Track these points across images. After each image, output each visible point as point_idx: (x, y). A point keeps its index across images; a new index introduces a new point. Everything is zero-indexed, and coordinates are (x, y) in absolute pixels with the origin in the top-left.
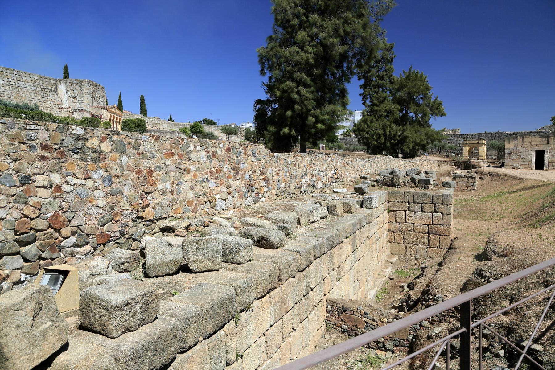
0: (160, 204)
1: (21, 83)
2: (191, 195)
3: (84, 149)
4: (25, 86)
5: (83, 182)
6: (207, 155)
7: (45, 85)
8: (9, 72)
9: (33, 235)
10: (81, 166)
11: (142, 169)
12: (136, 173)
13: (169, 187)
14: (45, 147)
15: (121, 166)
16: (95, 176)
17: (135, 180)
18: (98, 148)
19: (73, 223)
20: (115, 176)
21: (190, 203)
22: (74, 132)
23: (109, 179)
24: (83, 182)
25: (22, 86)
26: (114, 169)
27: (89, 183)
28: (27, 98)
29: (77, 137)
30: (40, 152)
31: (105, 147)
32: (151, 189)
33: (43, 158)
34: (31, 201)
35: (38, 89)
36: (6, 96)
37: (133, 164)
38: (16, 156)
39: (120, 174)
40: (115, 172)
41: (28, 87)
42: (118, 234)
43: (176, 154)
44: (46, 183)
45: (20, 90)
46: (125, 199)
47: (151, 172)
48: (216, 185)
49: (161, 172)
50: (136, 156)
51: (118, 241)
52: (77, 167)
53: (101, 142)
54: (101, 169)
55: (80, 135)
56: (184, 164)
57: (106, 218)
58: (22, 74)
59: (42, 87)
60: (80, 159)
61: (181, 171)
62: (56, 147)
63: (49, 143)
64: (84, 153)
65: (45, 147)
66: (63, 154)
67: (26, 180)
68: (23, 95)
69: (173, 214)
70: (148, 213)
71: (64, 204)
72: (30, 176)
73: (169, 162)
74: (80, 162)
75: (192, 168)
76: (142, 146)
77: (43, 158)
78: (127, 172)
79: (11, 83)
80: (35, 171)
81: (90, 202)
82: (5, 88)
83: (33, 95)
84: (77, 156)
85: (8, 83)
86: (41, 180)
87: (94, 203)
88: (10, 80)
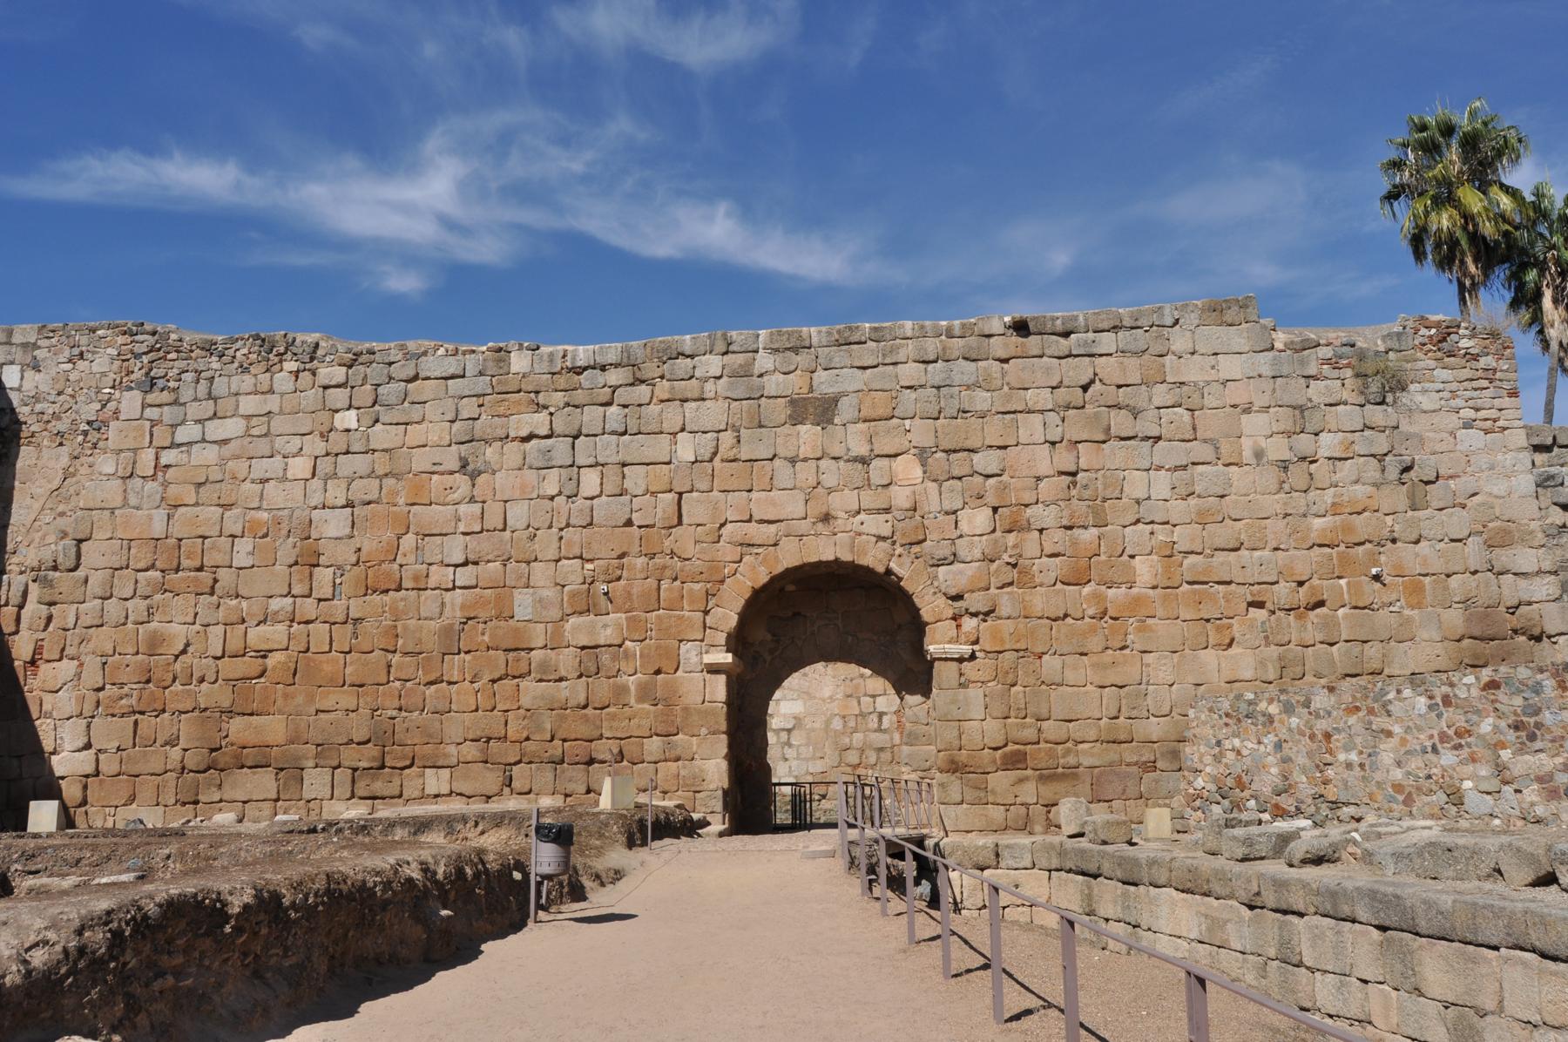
2: (1398, 774)
14: (1227, 715)
15: (1290, 730)
19: (1253, 786)
21: (1398, 788)
23: (1278, 746)
27: (1262, 748)
29: (1250, 703)
47: (1328, 736)
56: (1380, 722)
66: (1239, 720)
67: (1219, 743)
70: (1332, 793)
73: (1352, 720)
75: (1397, 729)
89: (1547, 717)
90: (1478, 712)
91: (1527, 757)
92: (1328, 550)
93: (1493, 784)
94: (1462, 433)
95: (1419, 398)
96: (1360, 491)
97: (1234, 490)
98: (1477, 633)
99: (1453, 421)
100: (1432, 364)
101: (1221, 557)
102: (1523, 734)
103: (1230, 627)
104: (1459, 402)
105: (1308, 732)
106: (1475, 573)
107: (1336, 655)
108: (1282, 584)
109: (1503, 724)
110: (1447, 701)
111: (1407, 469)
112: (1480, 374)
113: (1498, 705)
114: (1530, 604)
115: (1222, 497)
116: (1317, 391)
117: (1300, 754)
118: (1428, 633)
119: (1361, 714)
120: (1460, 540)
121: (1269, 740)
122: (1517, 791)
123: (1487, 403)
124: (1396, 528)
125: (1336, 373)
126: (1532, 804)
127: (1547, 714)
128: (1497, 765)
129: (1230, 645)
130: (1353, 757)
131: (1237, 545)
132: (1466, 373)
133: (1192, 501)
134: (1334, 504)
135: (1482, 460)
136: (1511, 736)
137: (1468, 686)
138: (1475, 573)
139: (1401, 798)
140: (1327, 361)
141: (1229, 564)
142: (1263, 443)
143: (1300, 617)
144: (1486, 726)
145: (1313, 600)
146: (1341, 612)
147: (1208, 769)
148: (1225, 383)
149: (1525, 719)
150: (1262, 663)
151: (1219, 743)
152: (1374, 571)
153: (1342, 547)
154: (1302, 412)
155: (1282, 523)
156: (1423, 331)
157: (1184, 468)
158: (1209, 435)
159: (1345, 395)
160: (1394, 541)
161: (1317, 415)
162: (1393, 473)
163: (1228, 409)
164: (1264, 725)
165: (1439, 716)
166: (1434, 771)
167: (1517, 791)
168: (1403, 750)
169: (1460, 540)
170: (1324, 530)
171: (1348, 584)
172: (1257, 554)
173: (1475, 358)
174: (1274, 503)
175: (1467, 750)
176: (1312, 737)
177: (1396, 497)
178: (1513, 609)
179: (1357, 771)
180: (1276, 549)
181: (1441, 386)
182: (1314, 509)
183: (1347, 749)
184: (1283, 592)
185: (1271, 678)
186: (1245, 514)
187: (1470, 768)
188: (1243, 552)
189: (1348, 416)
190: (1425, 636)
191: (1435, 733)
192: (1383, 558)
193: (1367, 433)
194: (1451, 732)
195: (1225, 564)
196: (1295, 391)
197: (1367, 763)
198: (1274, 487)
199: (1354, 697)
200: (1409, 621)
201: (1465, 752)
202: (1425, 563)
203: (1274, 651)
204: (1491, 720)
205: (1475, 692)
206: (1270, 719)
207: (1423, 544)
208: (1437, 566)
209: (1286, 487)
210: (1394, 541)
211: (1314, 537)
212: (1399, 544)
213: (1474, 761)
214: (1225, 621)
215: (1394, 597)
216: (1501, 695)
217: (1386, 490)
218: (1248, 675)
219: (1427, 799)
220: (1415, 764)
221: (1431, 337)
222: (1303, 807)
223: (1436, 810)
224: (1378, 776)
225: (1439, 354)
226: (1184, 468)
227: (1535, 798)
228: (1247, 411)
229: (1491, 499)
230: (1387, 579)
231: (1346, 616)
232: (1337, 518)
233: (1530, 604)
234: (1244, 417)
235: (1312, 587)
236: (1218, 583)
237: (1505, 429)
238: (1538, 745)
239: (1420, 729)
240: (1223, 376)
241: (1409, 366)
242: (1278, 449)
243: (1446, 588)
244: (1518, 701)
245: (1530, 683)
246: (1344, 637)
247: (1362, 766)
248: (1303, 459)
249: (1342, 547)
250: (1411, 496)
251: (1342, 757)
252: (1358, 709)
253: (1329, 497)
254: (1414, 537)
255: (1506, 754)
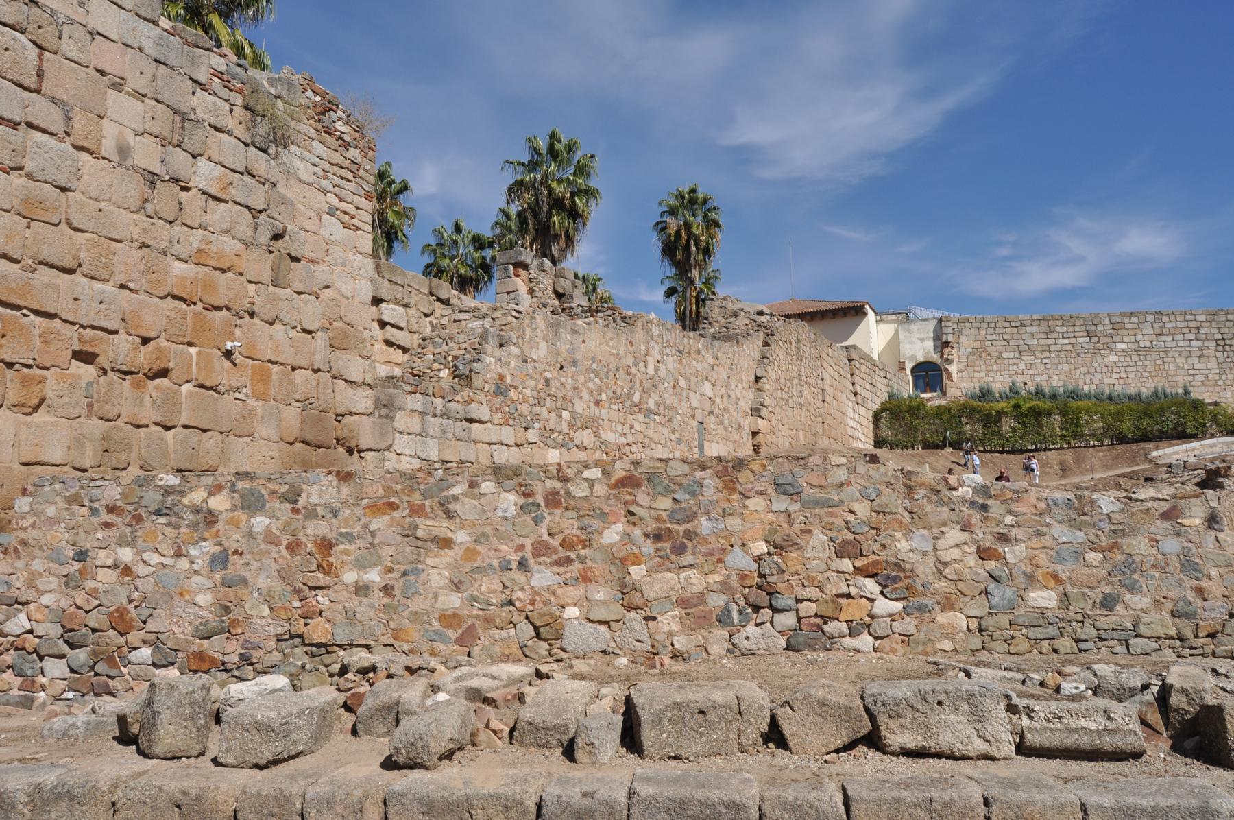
0: (350, 615)
1: (1164, 338)
2: (453, 601)
3: (176, 509)
4: (1174, 344)
5: (169, 561)
6: (522, 501)
7: (1225, 330)
8: (1135, 320)
9: (83, 635)
10: (169, 535)
11: (304, 539)
12: (287, 548)
13: (378, 579)
14: (111, 509)
15: (250, 535)
16: (193, 552)
17: (281, 561)
18: (204, 505)
19: (150, 626)
20: (236, 552)
21: (450, 619)
22: (160, 483)
23: (221, 560)
24: (169, 561)
25: (1168, 345)
26: (235, 540)
27: (183, 563)
28: (1181, 372)
29: (168, 491)
30: (105, 516)
31: (219, 503)
32: (322, 579)
33: (107, 525)
34: (90, 584)
35: (1206, 344)
36: (1132, 375)
37: (281, 531)
38: (72, 523)
39: (245, 548)
40: (235, 546)
41: (1181, 343)
42: (235, 659)
43: (406, 505)
44: (109, 562)
45: (1162, 355)
46: (256, 595)
47: (326, 546)
48: (561, 580)
49: (353, 547)
50: (291, 515)
51: (236, 673)
52: (161, 537)
53: (210, 494)
54: (205, 540)
55: (171, 487)
56: (429, 526)
57: (209, 626)
58: (1165, 319)
59: (1219, 336)
60: (168, 524)
61: (419, 543)
62: (130, 508)
63: (119, 503)
64: (176, 515)
65: (111, 509)
66: (138, 518)
67: (82, 556)
68: (1172, 367)
69: (392, 641)
70: (318, 631)
71: (136, 595)
72: (87, 551)
73: (378, 523)
74: (168, 530)
75: (461, 537)
76: (304, 495)
77: (107, 525)
78: (263, 546)
79: (1142, 344)
80: (96, 544)
81: (181, 594)
82: (1128, 359)
83: (1196, 360)
84: (162, 520)
85: (1135, 346)
86: (103, 557)
87: (187, 598)
88: (1139, 338)
89: (705, 525)
90: (603, 516)
91: (667, 575)
92: (181, 305)
93: (615, 611)
94: (326, 217)
95: (298, 163)
96: (230, 245)
97: (80, 186)
98: (309, 438)
99: (321, 202)
100: (313, 133)
101: (46, 274)
102: (667, 545)
103: (42, 381)
104: (326, 184)
105: (285, 539)
106: (316, 371)
107: (170, 442)
108: (122, 336)
109: (637, 532)
110: (553, 500)
111: (277, 237)
112: (347, 163)
113: (633, 508)
114: (351, 414)
115: (64, 189)
116: (202, 103)
117: (264, 576)
118: (267, 431)
119: (397, 515)
120: (309, 332)
121: (202, 552)
122: (647, 619)
123: (350, 197)
124: (257, 300)
125: (225, 93)
126: (670, 634)
127: (704, 520)
128: (624, 585)
129: (36, 409)
130: (374, 576)
131: (73, 265)
132: (337, 158)
133: (17, 179)
134: (200, 250)
135: (337, 253)
136: (648, 547)
137: (591, 483)
138: (316, 371)
139: (452, 634)
140: (218, 74)
141: (57, 288)
142: (131, 139)
143: (137, 386)
144: (612, 535)
145: (157, 366)
146: (186, 388)
147: (46, 600)
148: (94, 34)
149: (671, 526)
150: (79, 441)
151: (82, 556)
152: (229, 345)
153: (200, 306)
154: (183, 121)
155: (136, 254)
156: (309, 94)
157: (15, 125)
158: (59, 93)
159: (231, 124)
160: (252, 315)
161: (199, 134)
162: (264, 236)
163: (91, 71)
164: (194, 526)
165: (537, 521)
166: (520, 594)
167: (647, 619)
168: (468, 567)
169: (309, 332)
170: (184, 278)
171: (199, 354)
172: (98, 286)
173: (346, 145)
174: (130, 224)
175: (578, 565)
176: (294, 547)
177: (259, 265)
178: (340, 416)
179: (377, 598)
180: (123, 287)
181: (317, 160)
182: (177, 249)
183: (361, 565)
184: (121, 348)
185: (87, 463)
186: (90, 226)
187: (578, 591)
188: (78, 277)
189: (230, 149)
190: (264, 433)
191: (528, 543)
192: (238, 332)
193: (247, 178)
194: (554, 542)
195: (48, 287)
196: (178, 91)
197: (398, 586)
198: (135, 203)
199: (388, 490)
200: (252, 412)
201: (574, 569)
202: (276, 349)
203: (96, 427)
204: (620, 527)
205: (600, 490)
206: (211, 518)
207: (277, 326)
208: (287, 356)
209: (150, 208)
210: (252, 315)
211: (170, 285)
212: (256, 320)
213: (586, 580)
214: (36, 371)
215: (242, 382)
216: (642, 496)
217: (256, 253)
218: (56, 455)
219: (497, 634)
220: (488, 586)
221: (315, 104)
222: (256, 654)
223: (515, 649)
224: (417, 604)
225: (320, 126)
226: (15, 125)
227: (675, 627)
228: (118, 86)
229: (339, 297)
230: (239, 359)
231: (190, 393)
232: (199, 268)
233: (351, 414)
234: (112, 94)
235: (158, 348)
236: (37, 313)
237: (359, 229)
238: (688, 559)
239: (502, 538)
240: (94, 23)
241: (293, 124)
242: (147, 155)
243: (290, 382)
244: (665, 503)
245: (685, 482)
246: (183, 421)
247: (387, 590)
248: (175, 180)
249: (200, 306)
250: (276, 269)
251: (350, 577)
252: (392, 506)
253: (195, 239)
254: (270, 318)
255: (637, 572)
